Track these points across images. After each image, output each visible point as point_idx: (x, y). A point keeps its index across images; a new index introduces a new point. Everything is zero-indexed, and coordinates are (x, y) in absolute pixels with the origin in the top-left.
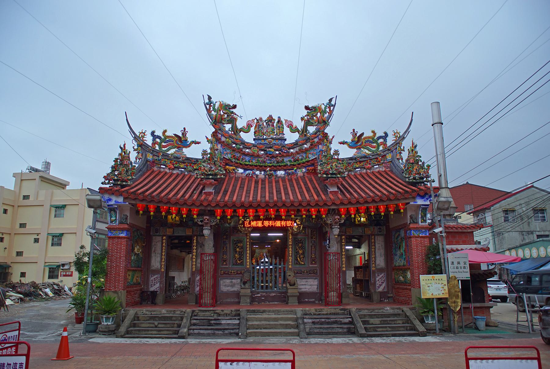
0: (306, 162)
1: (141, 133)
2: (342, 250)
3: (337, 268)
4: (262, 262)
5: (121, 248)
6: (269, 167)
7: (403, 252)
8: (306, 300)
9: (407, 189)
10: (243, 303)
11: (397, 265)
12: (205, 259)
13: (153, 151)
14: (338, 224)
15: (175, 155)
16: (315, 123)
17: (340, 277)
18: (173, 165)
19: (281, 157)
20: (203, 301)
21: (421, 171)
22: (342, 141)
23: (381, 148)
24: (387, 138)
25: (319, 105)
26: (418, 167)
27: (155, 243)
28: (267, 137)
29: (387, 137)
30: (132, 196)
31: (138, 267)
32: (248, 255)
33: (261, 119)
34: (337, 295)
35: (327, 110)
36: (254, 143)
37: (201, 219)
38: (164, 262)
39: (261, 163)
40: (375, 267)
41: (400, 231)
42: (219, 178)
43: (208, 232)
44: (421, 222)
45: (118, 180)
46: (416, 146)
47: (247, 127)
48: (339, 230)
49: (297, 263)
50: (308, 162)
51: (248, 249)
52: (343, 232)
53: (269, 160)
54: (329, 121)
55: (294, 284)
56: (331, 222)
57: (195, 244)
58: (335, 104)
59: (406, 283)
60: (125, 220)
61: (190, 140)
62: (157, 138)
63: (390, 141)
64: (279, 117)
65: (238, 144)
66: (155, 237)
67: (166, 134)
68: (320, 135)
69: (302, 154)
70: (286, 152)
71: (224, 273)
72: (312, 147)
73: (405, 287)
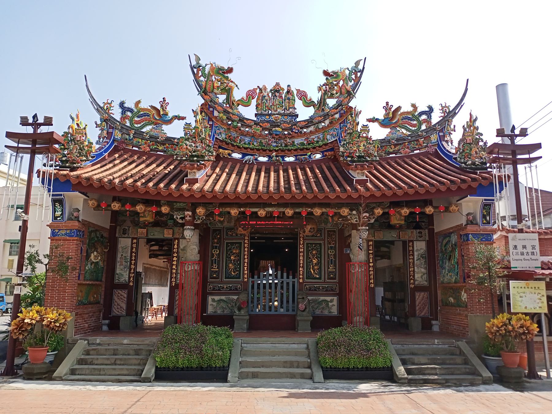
0: (323, 145)
4: (265, 276)
6: (276, 151)
12: (186, 269)
13: (124, 129)
15: (152, 133)
16: (336, 94)
18: (149, 146)
19: (290, 138)
21: (482, 154)
22: (372, 117)
23: (423, 127)
24: (432, 114)
26: (478, 148)
28: (273, 112)
29: (431, 113)
31: (97, 280)
34: (364, 321)
35: (352, 76)
36: (256, 120)
37: (181, 216)
45: (67, 161)
46: (476, 120)
47: (247, 99)
50: (326, 145)
53: (275, 142)
54: (355, 92)
56: (356, 221)
58: (364, 68)
61: (170, 115)
62: (128, 111)
63: (436, 118)
64: (289, 86)
65: (235, 121)
67: (140, 105)
69: (318, 135)
70: (297, 131)
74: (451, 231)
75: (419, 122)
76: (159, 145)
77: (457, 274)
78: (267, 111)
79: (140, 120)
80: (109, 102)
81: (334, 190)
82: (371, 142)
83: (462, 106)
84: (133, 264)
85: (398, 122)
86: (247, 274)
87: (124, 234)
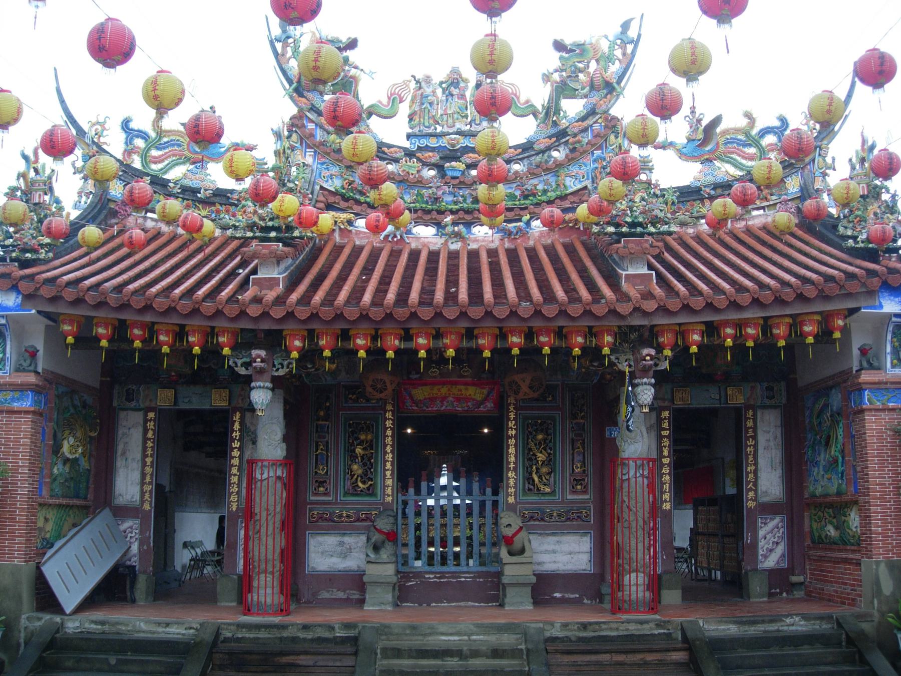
0: (556, 198)
1: (94, 125)
2: (662, 452)
3: (647, 505)
5: (17, 441)
6: (452, 212)
7: (837, 454)
8: (557, 595)
9: (851, 269)
10: (373, 605)
11: (819, 491)
14: (651, 373)
16: (583, 89)
17: (655, 529)
20: (253, 598)
21: (888, 218)
25: (594, 41)
26: (879, 207)
27: (126, 431)
28: (446, 130)
30: (46, 292)
31: (77, 496)
32: (388, 466)
33: (428, 80)
34: (647, 582)
35: (615, 52)
37: (244, 360)
38: (150, 483)
39: (427, 203)
40: (755, 499)
41: (828, 395)
42: (297, 237)
43: (263, 397)
44: (893, 366)
47: (389, 104)
48: (653, 390)
49: (529, 490)
51: (389, 449)
52: (663, 400)
53: (450, 193)
55: (522, 551)
57: (236, 434)
58: (639, 36)
59: (845, 543)
60: (28, 362)
62: (137, 136)
66: (125, 413)
68: (596, 122)
69: (545, 178)
71: (321, 518)
72: (574, 155)
73: (844, 555)
74: (831, 383)
75: (760, 150)
76: (200, 207)
77: (842, 476)
78: (433, 128)
79: (163, 155)
80: (101, 120)
81: (677, 294)
82: (658, 192)
83: (846, 116)
84: (148, 463)
85: (716, 150)
86: (393, 486)
87: (129, 400)
